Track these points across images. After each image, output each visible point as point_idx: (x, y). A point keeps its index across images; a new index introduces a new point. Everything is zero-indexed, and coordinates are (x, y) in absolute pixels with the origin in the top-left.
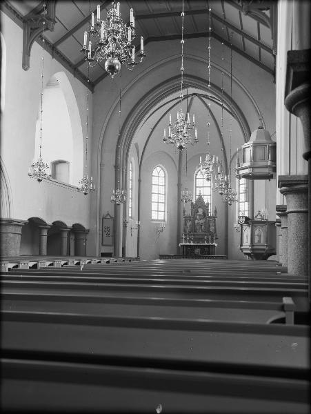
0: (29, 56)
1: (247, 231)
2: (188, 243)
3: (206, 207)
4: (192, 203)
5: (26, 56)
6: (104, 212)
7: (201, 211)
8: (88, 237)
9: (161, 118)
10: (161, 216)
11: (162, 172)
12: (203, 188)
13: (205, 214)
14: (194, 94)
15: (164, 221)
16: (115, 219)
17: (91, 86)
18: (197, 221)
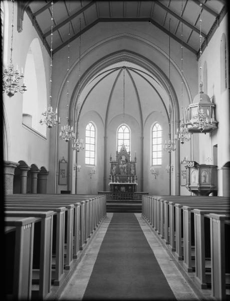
0: (22, 20)
1: (195, 173)
2: (115, 183)
3: (127, 156)
4: (117, 152)
5: (20, 20)
6: (60, 158)
7: (124, 158)
8: (48, 178)
9: (95, 86)
10: (159, 162)
11: (93, 127)
12: (124, 138)
13: (127, 161)
14: (124, 67)
15: (94, 165)
16: (69, 163)
17: (52, 54)
18: (120, 166)
